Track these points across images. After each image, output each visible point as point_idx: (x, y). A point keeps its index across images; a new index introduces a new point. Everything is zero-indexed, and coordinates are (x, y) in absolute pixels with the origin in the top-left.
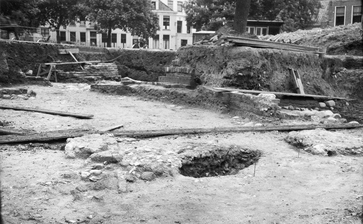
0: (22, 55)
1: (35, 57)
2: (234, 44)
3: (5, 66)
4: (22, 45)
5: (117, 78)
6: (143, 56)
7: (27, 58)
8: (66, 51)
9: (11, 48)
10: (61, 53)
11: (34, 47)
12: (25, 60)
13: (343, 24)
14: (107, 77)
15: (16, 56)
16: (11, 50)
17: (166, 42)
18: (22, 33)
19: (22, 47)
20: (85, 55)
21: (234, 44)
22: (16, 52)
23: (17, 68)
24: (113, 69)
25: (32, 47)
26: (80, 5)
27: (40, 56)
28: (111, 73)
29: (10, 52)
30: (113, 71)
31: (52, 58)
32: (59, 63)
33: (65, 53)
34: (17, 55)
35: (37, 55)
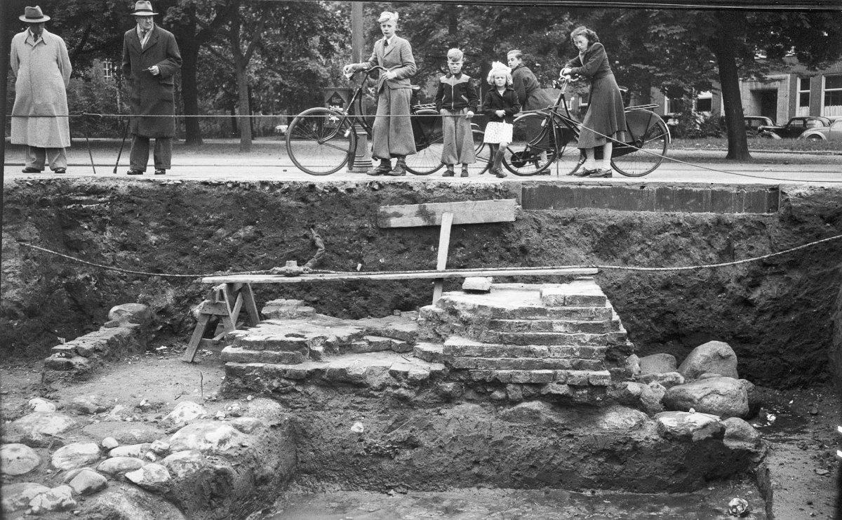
1: (248, 240)
2: (347, 165)
5: (563, 390)
6: (447, 337)
8: (423, 213)
9: (129, 207)
10: (394, 222)
11: (240, 201)
12: (196, 254)
13: (455, 228)
14: (477, 377)
15: (153, 238)
17: (345, 150)
19: (178, 202)
20: (587, 229)
21: (347, 165)
23: (155, 284)
25: (230, 202)
28: (530, 352)
30: (551, 340)
32: (298, 274)
33: (419, 222)
34: (156, 232)
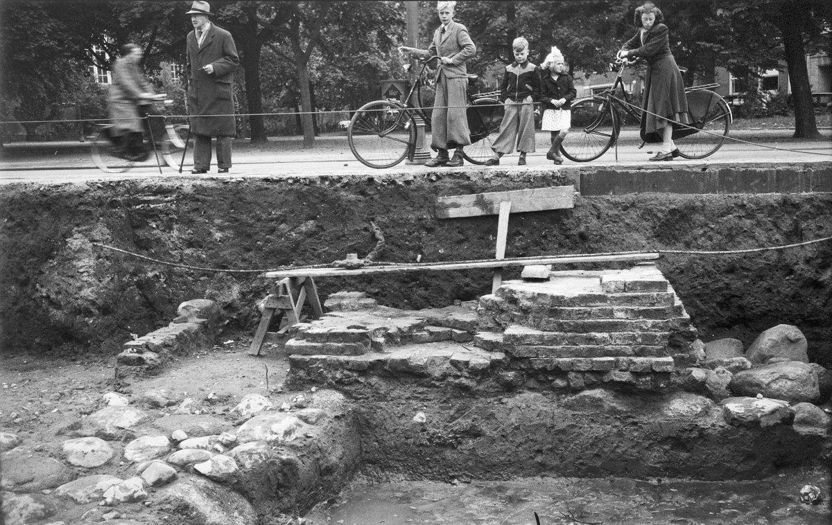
0: (243, 233)
1: (310, 234)
3: (78, 284)
4: (241, 191)
5: (626, 377)
7: (268, 241)
8: (480, 203)
10: (453, 213)
11: (300, 196)
13: (514, 217)
16: (193, 216)
18: (549, 77)
19: (241, 199)
20: (648, 213)
22: (218, 221)
24: (620, 316)
25: (291, 198)
26: (285, 92)
27: (331, 229)
28: (590, 340)
29: (192, 221)
31: (785, 202)
32: (359, 266)
33: (477, 212)
34: (221, 229)
35: (321, 228)
